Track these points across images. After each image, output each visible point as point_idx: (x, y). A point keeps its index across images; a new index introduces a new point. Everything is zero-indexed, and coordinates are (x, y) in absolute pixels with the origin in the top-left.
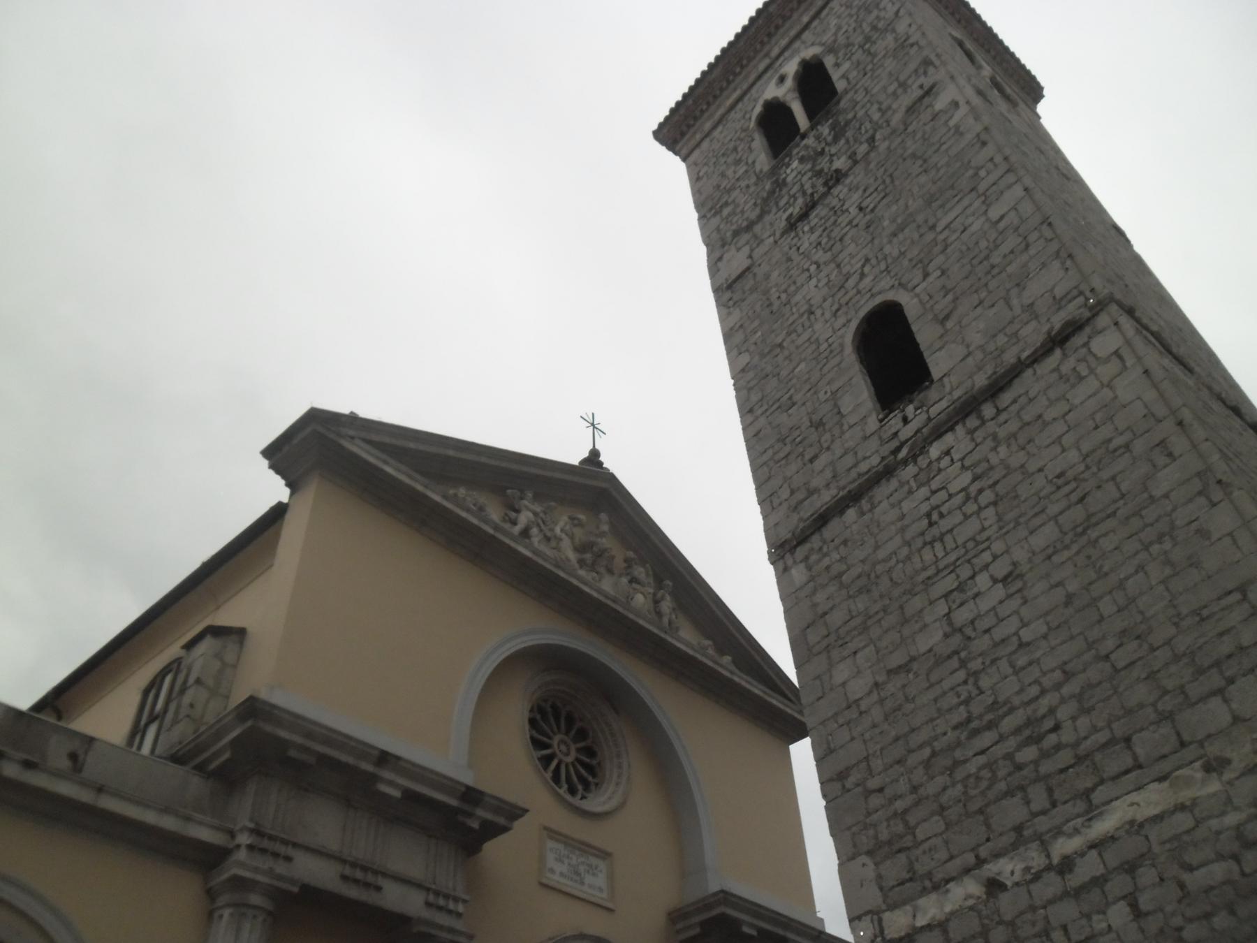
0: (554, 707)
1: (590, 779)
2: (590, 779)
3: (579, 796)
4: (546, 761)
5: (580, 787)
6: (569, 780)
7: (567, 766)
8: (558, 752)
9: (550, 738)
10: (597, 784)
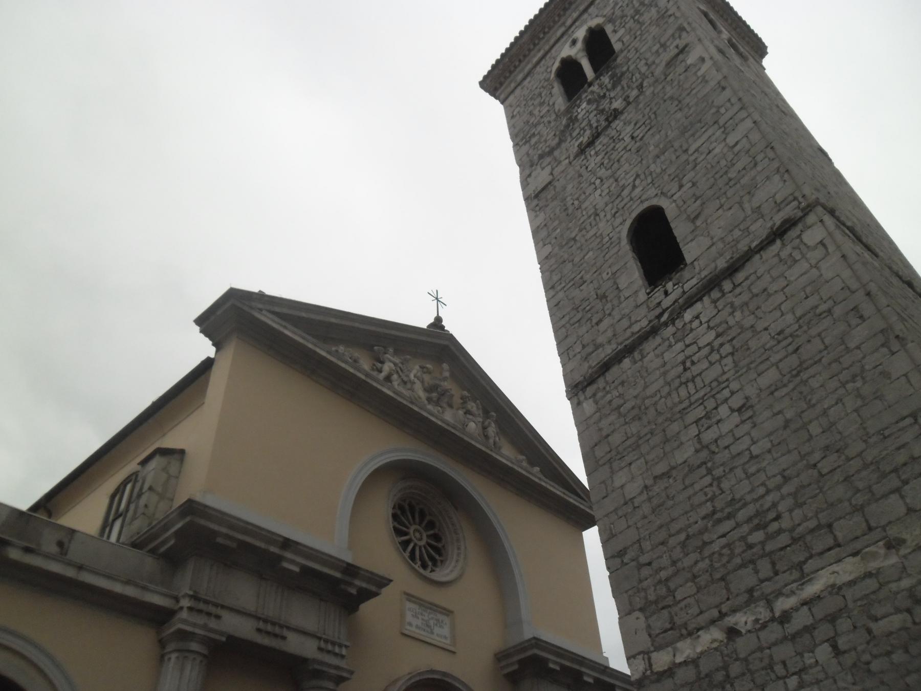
0: (410, 505)
1: (437, 557)
2: (437, 557)
3: (429, 569)
4: (405, 544)
5: (430, 563)
6: (422, 559)
7: (420, 547)
8: (413, 538)
9: (408, 528)
10: (442, 561)
